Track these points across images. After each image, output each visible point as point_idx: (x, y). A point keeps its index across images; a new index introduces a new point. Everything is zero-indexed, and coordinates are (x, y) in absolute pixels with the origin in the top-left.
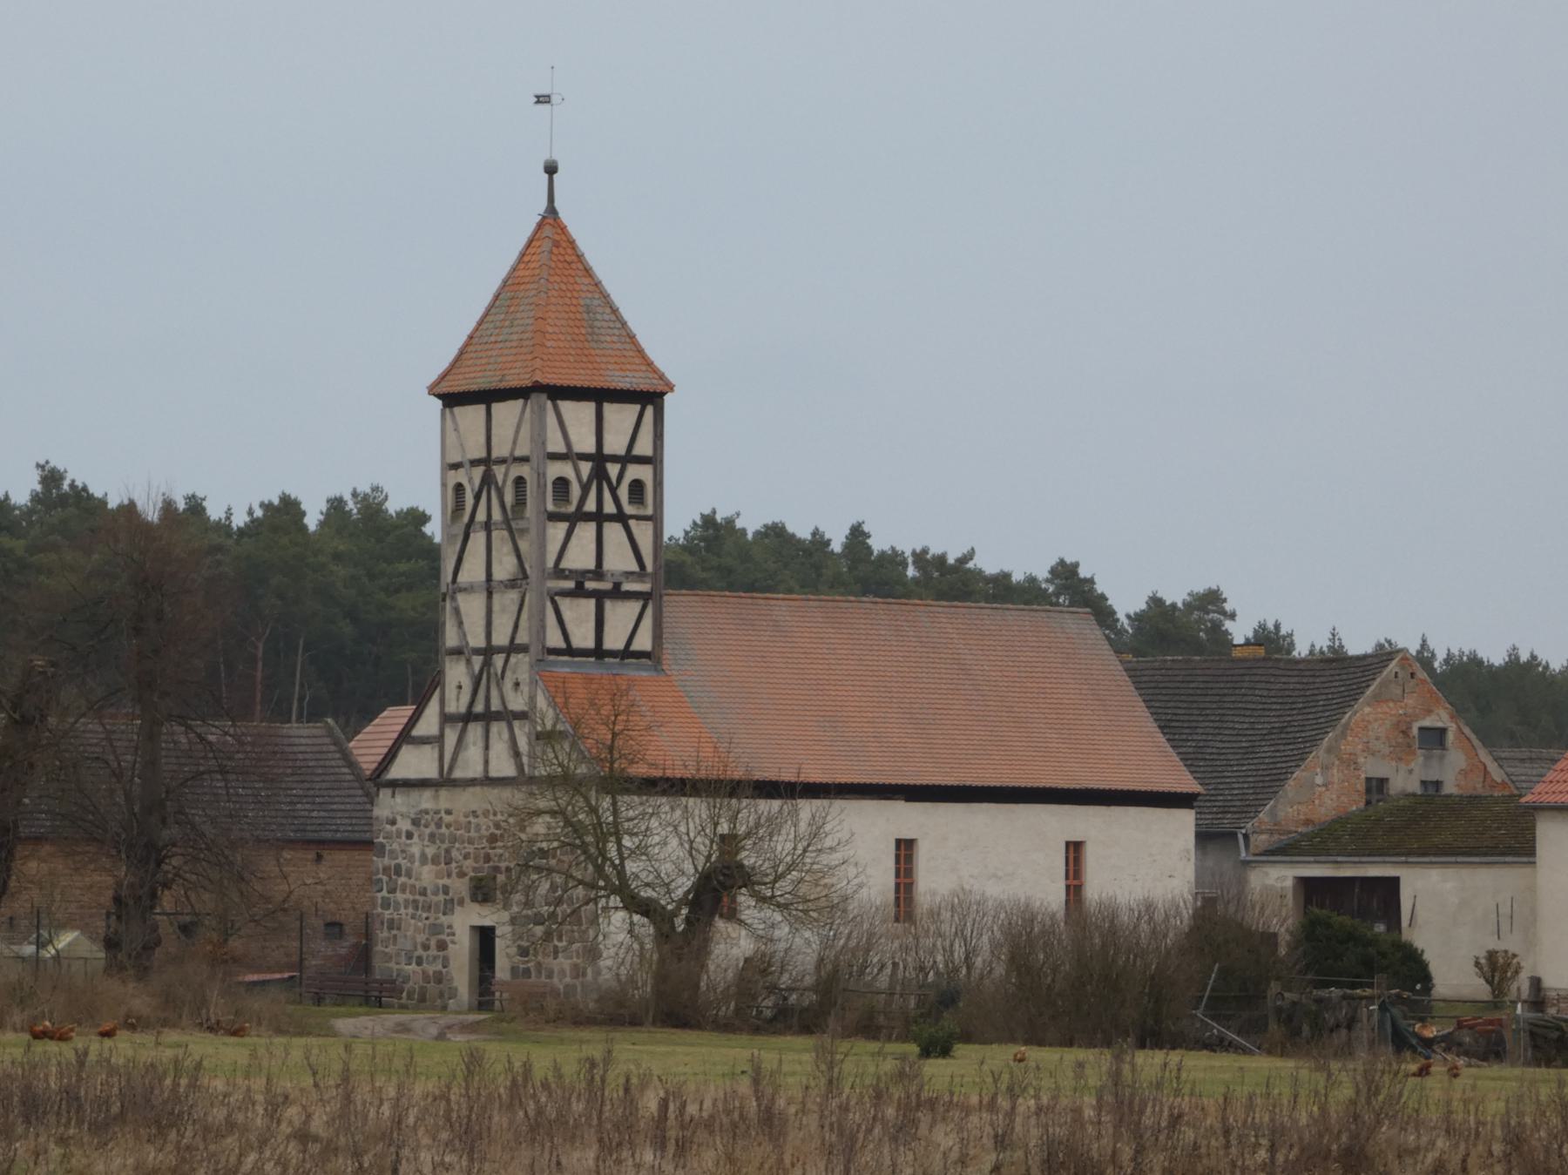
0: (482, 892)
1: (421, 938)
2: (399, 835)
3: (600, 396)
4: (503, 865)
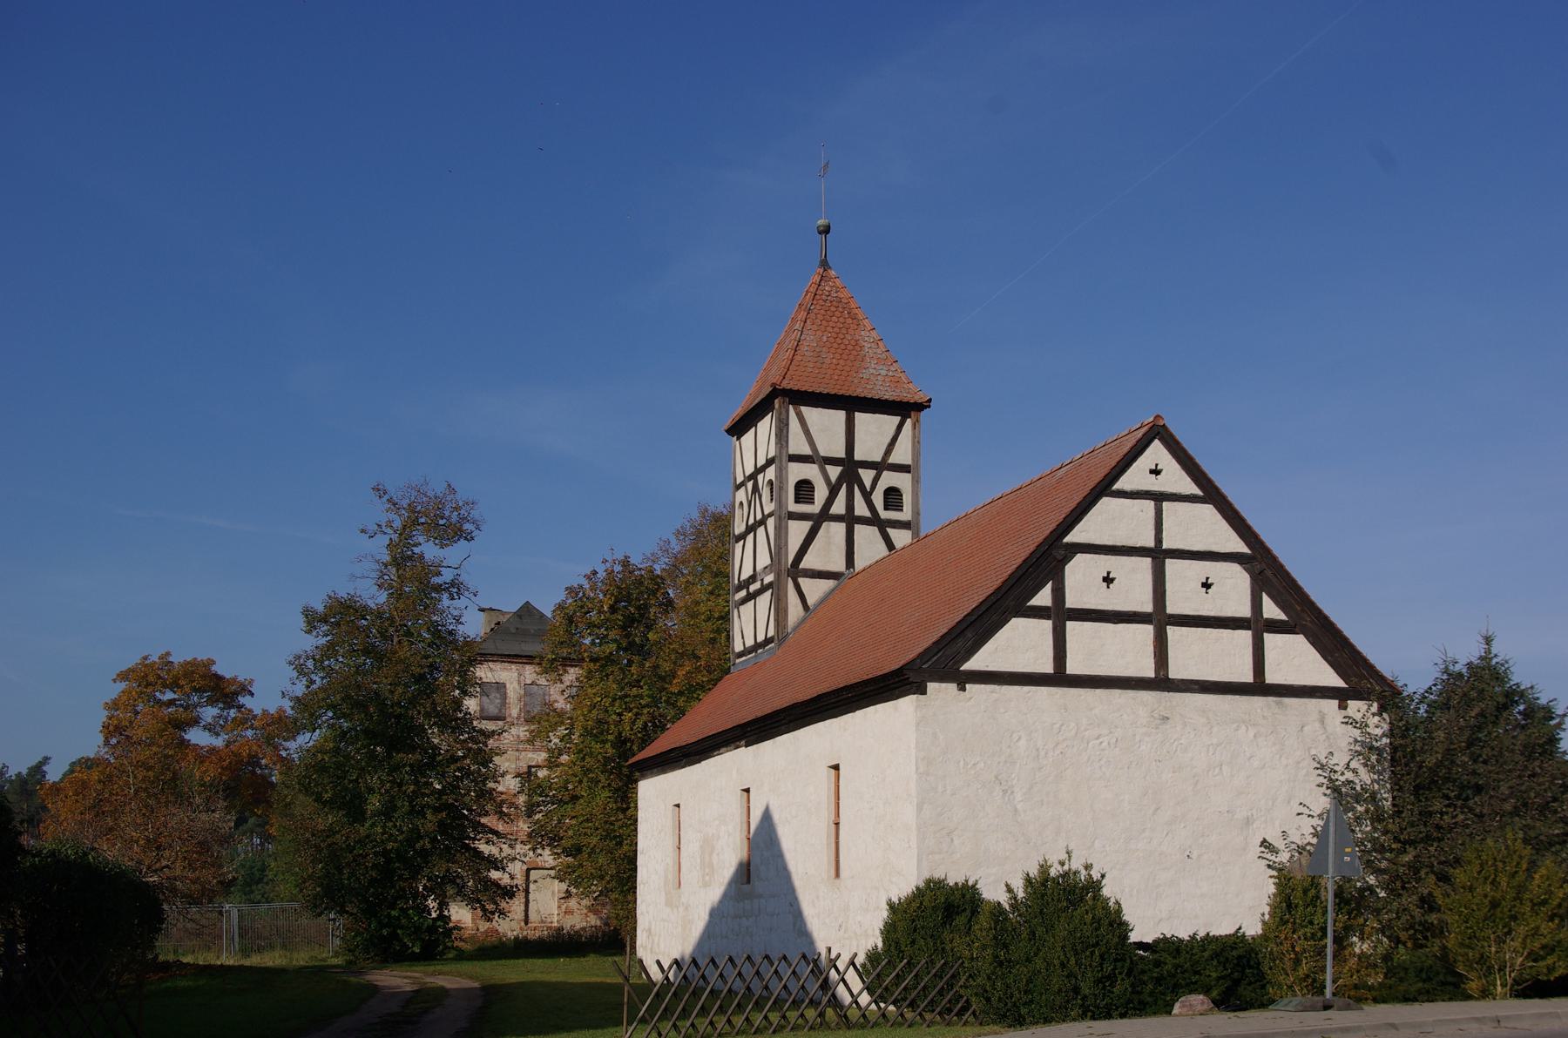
3: (852, 404)
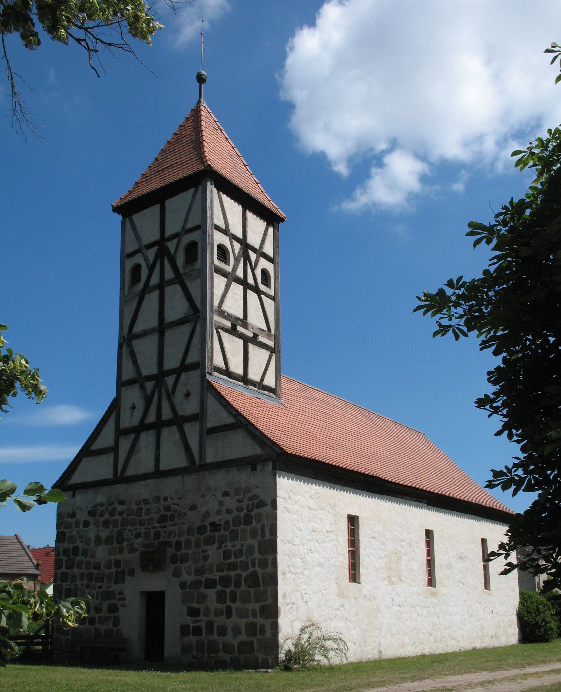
0: (152, 561)
4: (173, 540)
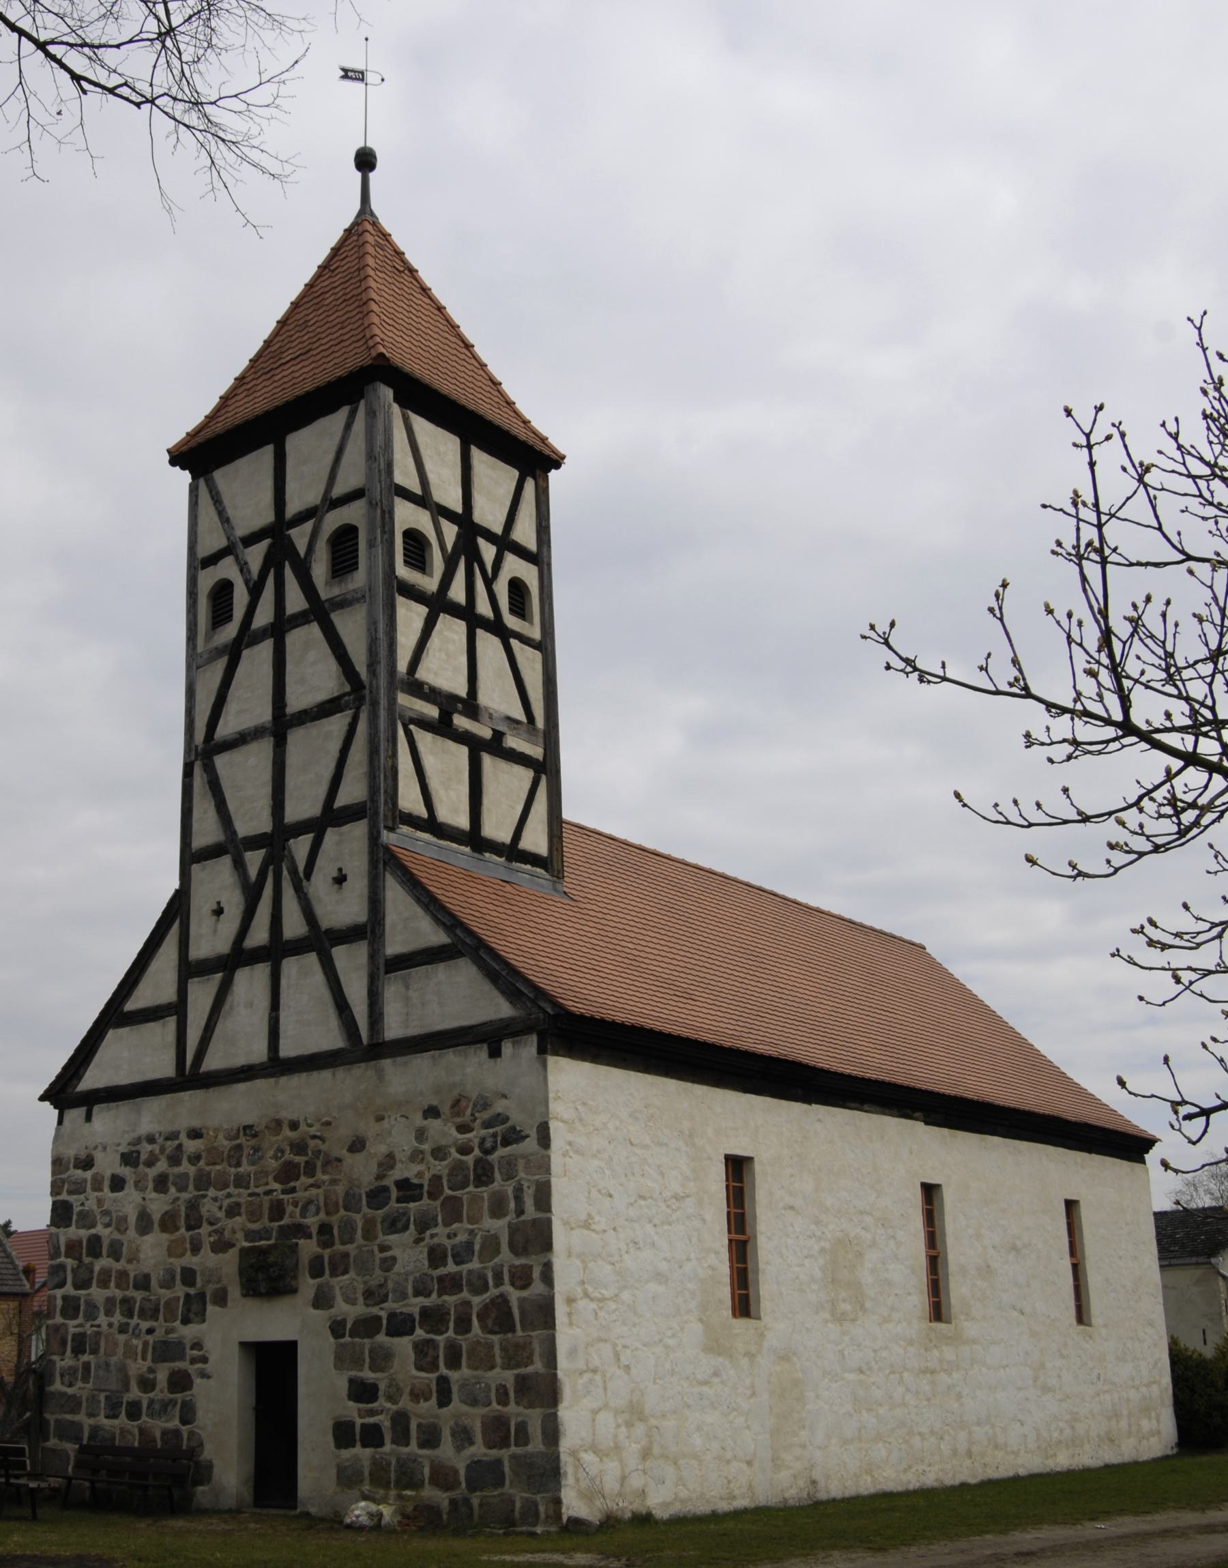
0: (266, 1277)
1: (137, 1367)
2: (97, 1187)
